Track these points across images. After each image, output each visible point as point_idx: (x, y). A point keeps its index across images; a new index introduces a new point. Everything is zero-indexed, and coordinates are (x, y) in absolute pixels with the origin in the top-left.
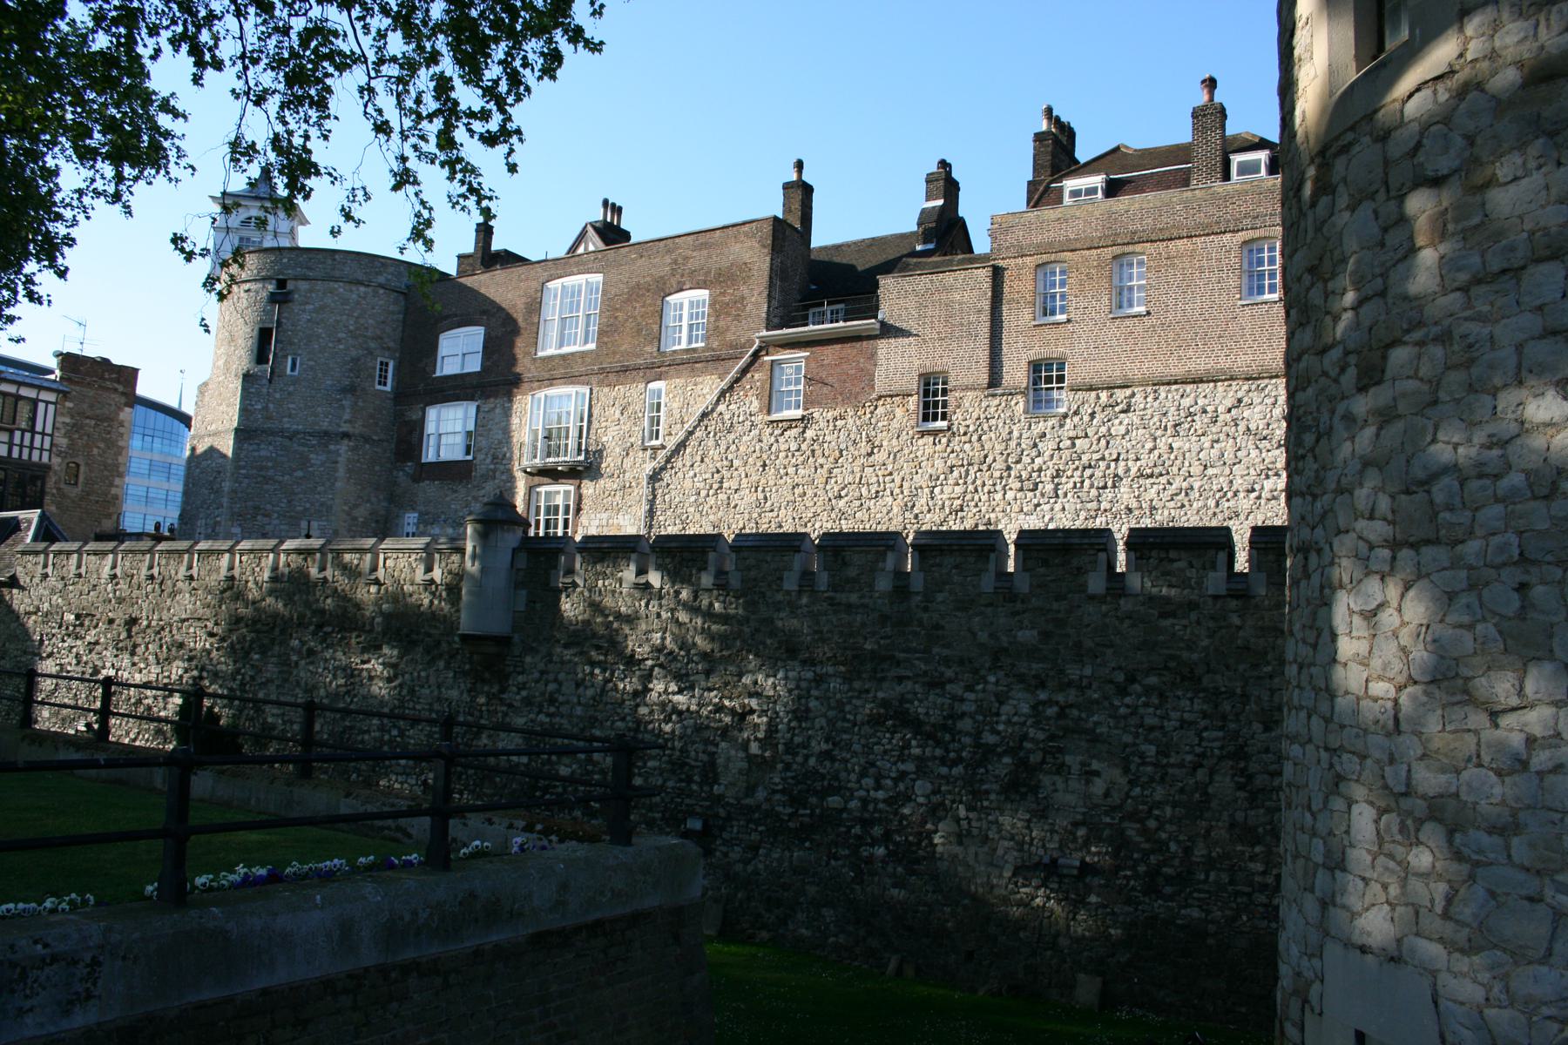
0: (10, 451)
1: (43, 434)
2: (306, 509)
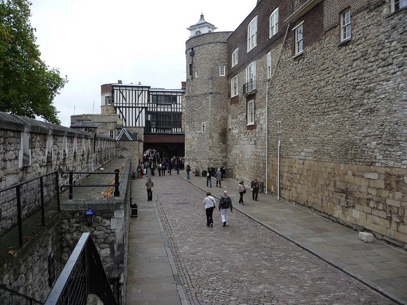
1: (179, 104)
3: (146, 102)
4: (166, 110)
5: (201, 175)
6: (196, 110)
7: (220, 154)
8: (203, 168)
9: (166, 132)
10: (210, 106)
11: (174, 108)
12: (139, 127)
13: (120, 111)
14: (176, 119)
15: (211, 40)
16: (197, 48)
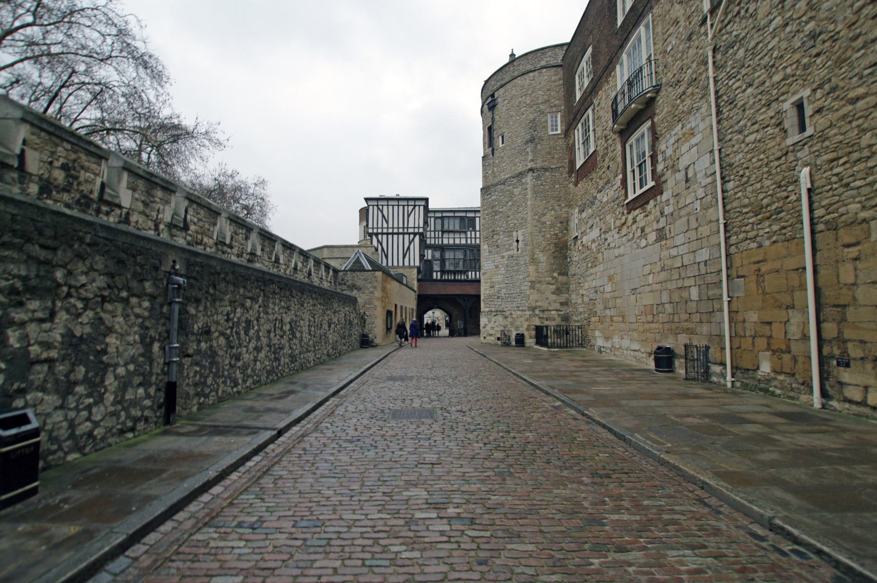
2: (515, 224)
3: (421, 225)
4: (457, 241)
5: (514, 343)
6: (501, 210)
7: (554, 297)
8: (517, 328)
9: (458, 277)
10: (529, 196)
12: (410, 267)
13: (378, 241)
14: (473, 254)
16: (502, 91)
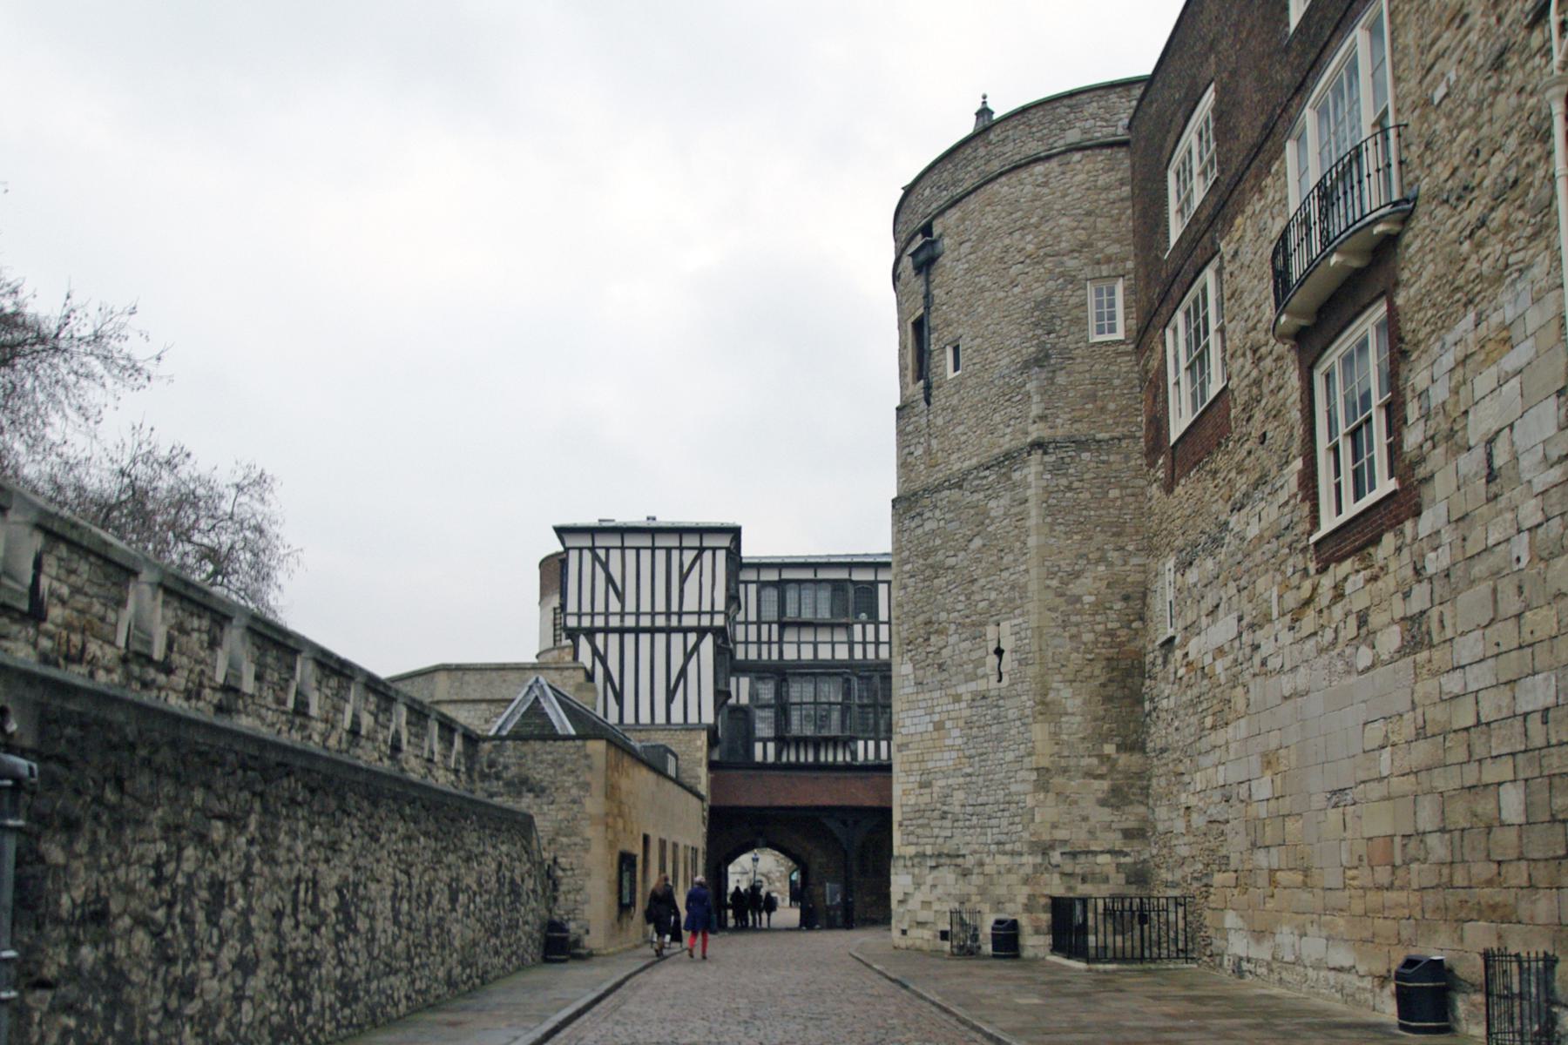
0: (851, 651)
2: (992, 604)
3: (720, 605)
4: (825, 653)
5: (988, 948)
6: (951, 561)
7: (1105, 814)
8: (998, 904)
9: (827, 756)
10: (1032, 522)
11: (864, 643)
12: (686, 727)
13: (595, 651)
15: (1033, 147)
16: (953, 215)
